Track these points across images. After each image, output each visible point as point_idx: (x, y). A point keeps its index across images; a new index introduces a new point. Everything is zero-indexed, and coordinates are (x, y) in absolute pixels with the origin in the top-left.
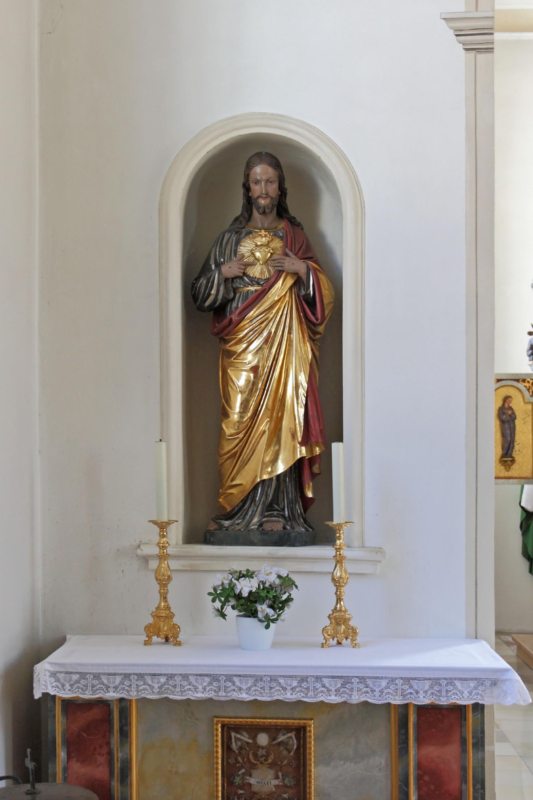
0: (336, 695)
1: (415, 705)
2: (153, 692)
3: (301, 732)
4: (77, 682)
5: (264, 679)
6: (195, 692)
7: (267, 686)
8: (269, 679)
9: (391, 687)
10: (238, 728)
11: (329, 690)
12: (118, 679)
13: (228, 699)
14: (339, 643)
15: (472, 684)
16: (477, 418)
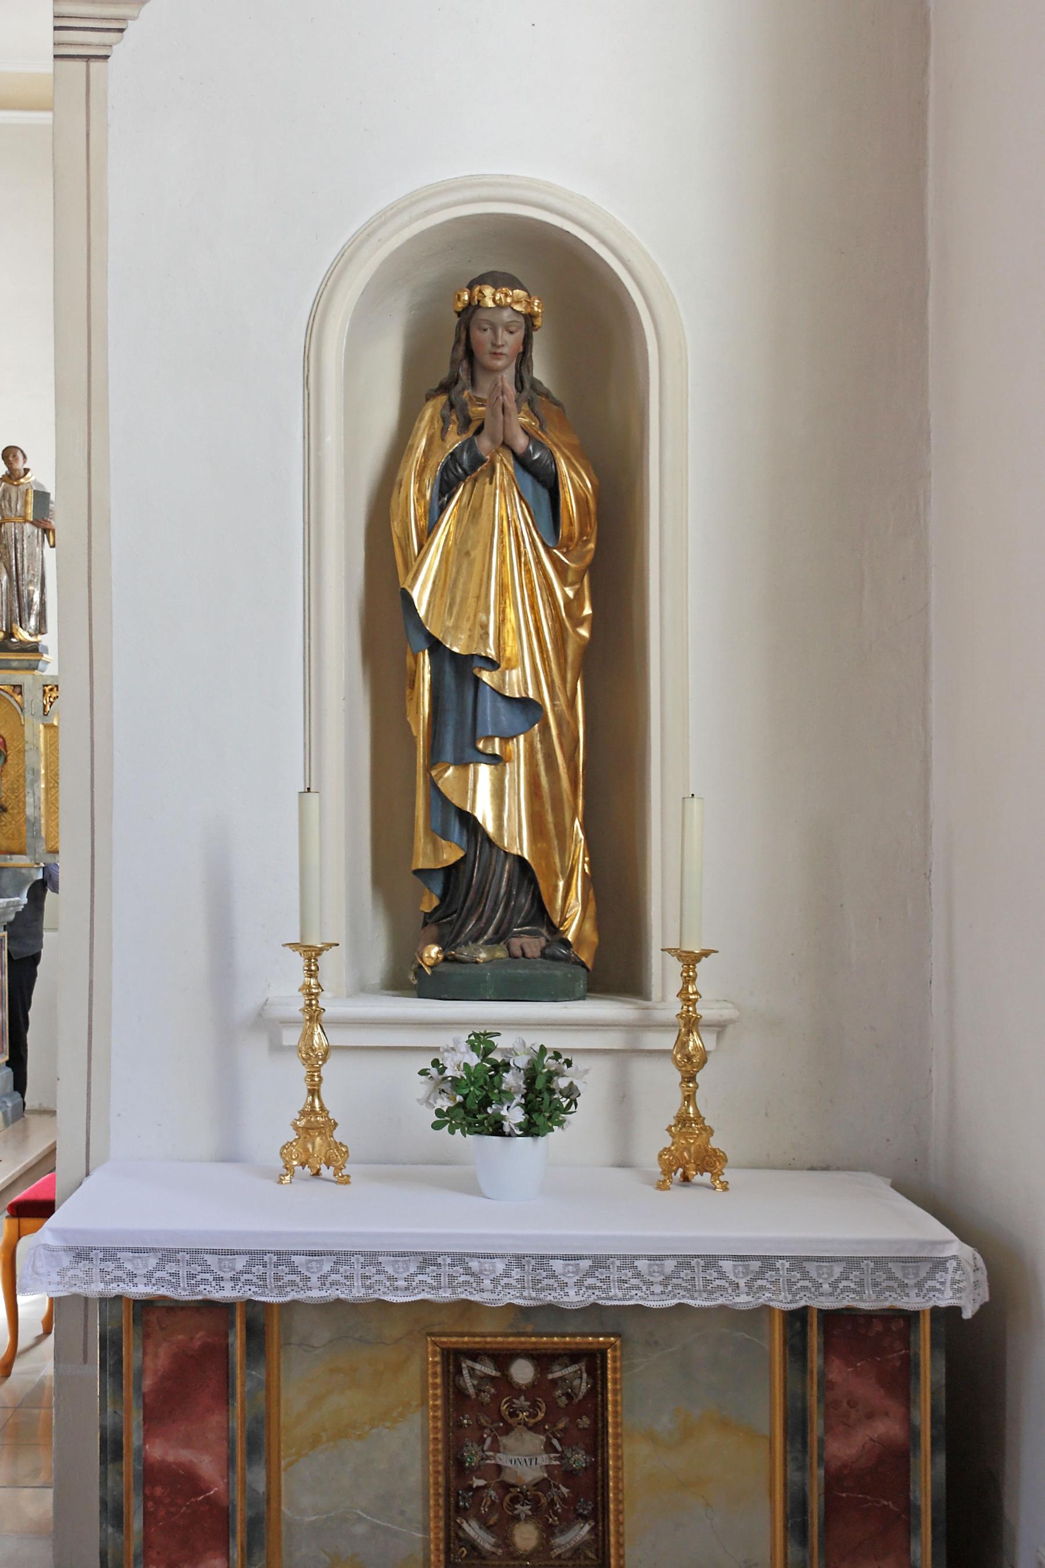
0: (748, 1294)
1: (820, 1311)
2: (653, 1293)
3: (594, 1361)
4: (675, 1274)
5: (92, 1255)
6: (131, 1284)
7: (358, 1270)
8: (275, 1259)
9: (851, 1277)
10: (474, 1355)
11: (904, 1286)
12: (241, 1262)
13: (539, 1303)
14: (686, 1179)
15: (755, 1265)
16: (88, 194)
